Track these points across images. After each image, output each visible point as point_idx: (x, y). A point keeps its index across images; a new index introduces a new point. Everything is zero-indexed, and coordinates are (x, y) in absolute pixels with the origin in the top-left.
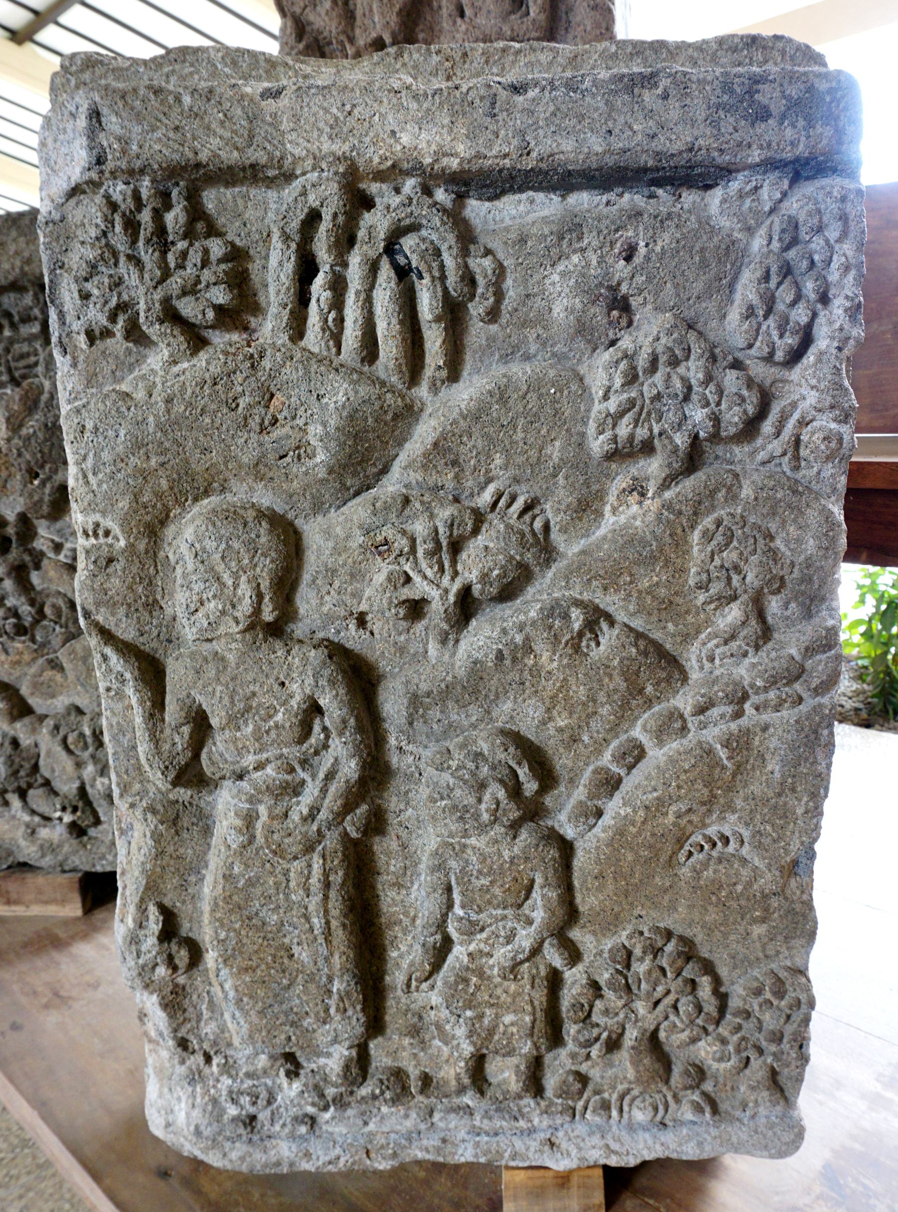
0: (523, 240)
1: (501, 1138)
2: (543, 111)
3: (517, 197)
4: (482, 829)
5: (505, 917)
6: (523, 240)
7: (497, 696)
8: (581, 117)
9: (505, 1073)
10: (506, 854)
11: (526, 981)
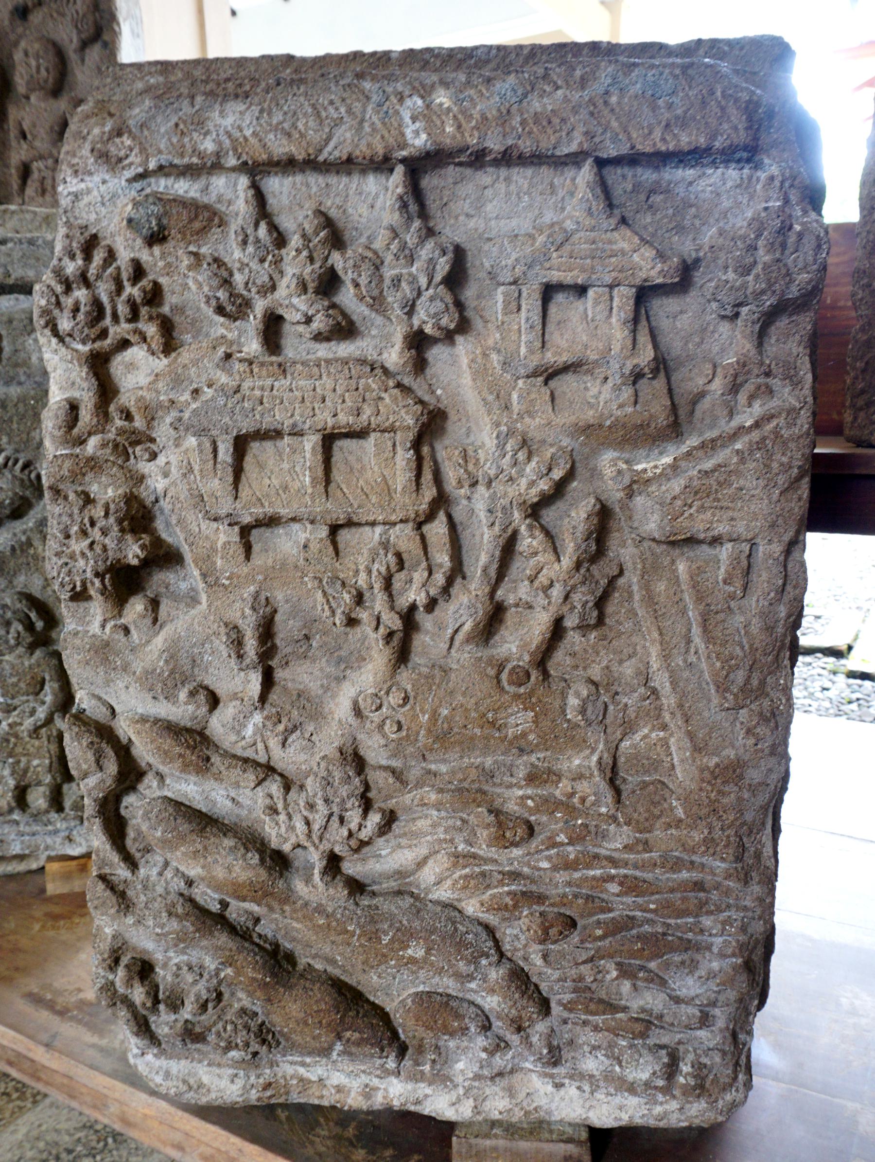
0: (10, 321)
1: (37, 837)
2: (17, 255)
3: (8, 297)
4: (11, 649)
5: (28, 701)
6: (10, 321)
7: (15, 573)
8: (38, 259)
9: (38, 799)
10: (27, 663)
11: (45, 739)
